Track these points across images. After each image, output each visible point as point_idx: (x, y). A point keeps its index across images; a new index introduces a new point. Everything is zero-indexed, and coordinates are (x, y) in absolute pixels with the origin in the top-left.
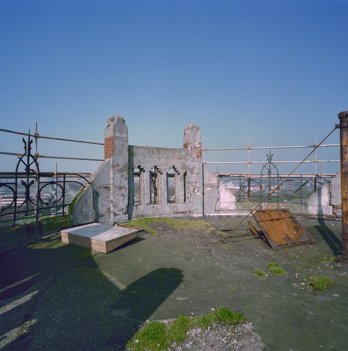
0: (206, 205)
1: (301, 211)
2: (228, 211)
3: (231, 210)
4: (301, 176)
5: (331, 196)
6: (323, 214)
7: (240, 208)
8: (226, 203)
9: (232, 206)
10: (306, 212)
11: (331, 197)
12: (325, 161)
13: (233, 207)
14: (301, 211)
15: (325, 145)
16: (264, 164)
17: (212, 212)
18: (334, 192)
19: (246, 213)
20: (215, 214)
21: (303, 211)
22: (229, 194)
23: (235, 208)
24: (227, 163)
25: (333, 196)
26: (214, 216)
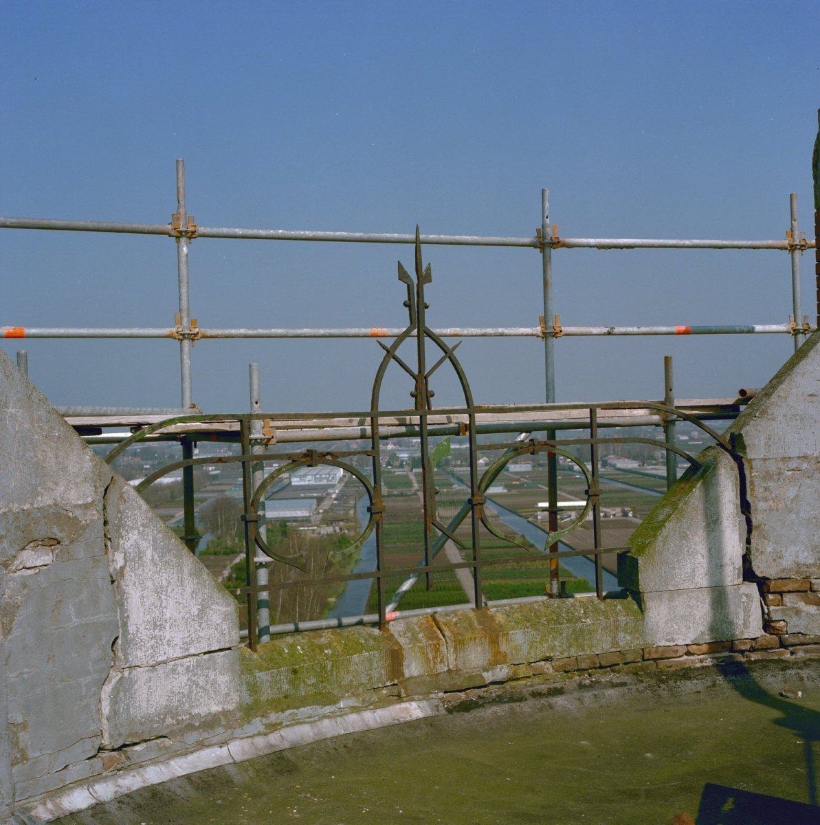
0: (24, 726)
1: (615, 642)
2: (192, 737)
3: (210, 723)
4: (592, 413)
5: (749, 521)
6: (707, 638)
7: (267, 694)
8: (174, 671)
9: (215, 682)
10: (639, 643)
11: (750, 531)
12: (595, 330)
13: (219, 692)
14: (615, 642)
15: (592, 241)
16: (389, 343)
17: (75, 772)
18: (766, 500)
19: (310, 720)
20: (105, 791)
21: (625, 640)
22: (190, 585)
23: (235, 697)
24: (28, 331)
25: (758, 527)
26: (98, 809)
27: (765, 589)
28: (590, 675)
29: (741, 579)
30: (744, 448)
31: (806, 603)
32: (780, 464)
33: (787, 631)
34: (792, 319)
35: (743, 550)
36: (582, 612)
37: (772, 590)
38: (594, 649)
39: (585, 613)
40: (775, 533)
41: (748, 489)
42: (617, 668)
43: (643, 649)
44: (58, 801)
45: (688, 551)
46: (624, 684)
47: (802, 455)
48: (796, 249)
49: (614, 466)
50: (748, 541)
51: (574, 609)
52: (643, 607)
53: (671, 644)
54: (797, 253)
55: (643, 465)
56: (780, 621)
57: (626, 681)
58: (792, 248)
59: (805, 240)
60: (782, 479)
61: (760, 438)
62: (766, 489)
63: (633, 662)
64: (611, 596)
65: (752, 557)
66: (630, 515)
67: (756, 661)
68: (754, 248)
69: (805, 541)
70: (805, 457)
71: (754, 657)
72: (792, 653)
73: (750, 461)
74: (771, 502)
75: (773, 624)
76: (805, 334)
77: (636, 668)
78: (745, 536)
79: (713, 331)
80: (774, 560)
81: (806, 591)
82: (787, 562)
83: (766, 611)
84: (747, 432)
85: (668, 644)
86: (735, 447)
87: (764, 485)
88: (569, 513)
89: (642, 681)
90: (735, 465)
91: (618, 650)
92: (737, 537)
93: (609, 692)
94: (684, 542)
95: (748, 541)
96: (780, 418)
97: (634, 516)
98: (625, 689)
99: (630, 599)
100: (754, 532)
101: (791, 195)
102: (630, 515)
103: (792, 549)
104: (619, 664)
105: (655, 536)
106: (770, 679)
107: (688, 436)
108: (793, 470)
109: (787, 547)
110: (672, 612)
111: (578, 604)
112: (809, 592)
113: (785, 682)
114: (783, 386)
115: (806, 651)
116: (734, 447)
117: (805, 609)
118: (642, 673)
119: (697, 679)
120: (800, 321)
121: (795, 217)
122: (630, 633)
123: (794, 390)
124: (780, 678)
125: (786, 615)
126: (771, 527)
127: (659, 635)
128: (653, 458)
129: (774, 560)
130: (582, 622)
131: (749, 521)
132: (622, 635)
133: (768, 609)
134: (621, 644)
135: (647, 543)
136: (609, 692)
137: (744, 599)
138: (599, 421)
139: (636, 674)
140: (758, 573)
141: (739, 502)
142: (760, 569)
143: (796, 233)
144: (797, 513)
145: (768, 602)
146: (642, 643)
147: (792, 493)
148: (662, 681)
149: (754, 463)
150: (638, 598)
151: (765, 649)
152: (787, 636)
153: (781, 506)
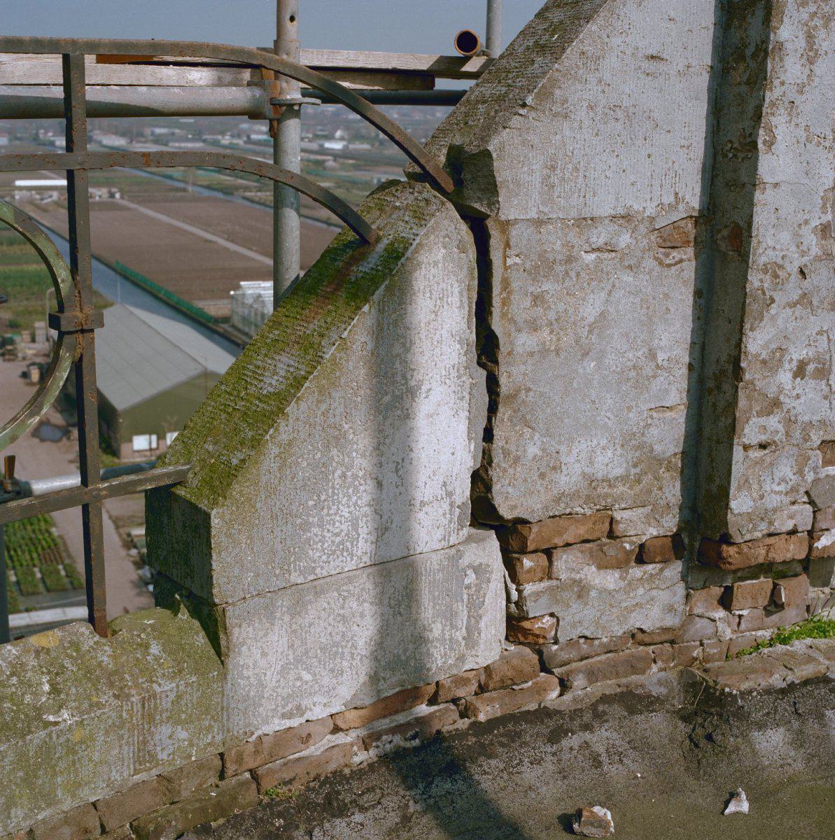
1: (144, 756)
5: (492, 384)
11: (493, 409)
14: (144, 756)
18: (534, 327)
21: (175, 743)
25: (512, 397)
27: (514, 544)
30: (491, 189)
31: (600, 567)
35: (474, 457)
36: (47, 688)
37: (531, 548)
39: (55, 690)
40: (549, 411)
41: (496, 301)
45: (344, 476)
47: (621, 211)
49: (100, 143)
50: (488, 435)
51: (21, 682)
52: (223, 643)
53: (295, 722)
55: (131, 142)
60: (573, 274)
62: (538, 299)
65: (494, 473)
66: (118, 196)
67: (493, 723)
69: (610, 423)
70: (626, 217)
73: (505, 226)
75: (526, 625)
78: (483, 423)
80: (542, 476)
82: (568, 479)
83: (515, 595)
84: (501, 149)
85: (288, 723)
86: (467, 182)
87: (531, 289)
88: (50, 193)
90: (464, 232)
92: (462, 427)
94: (334, 452)
95: (488, 435)
96: (582, 114)
97: (122, 197)
99: (184, 615)
100: (501, 409)
102: (118, 196)
103: (582, 446)
105: (257, 443)
106: (530, 774)
107: (320, 142)
108: (598, 250)
109: (572, 440)
110: (297, 643)
111: (32, 662)
112: (604, 540)
114: (593, 27)
116: (459, 183)
117: (597, 581)
119: (363, 809)
123: (616, 41)
126: (542, 395)
128: (142, 135)
130: (47, 724)
131: (492, 384)
133: (520, 592)
134: (163, 756)
135: (235, 461)
137: (471, 578)
138: (93, 95)
140: (506, 512)
142: (507, 504)
146: (219, 738)
147: (590, 311)
149: (514, 232)
150: (212, 622)
151: (507, 685)
152: (555, 647)
153: (567, 340)
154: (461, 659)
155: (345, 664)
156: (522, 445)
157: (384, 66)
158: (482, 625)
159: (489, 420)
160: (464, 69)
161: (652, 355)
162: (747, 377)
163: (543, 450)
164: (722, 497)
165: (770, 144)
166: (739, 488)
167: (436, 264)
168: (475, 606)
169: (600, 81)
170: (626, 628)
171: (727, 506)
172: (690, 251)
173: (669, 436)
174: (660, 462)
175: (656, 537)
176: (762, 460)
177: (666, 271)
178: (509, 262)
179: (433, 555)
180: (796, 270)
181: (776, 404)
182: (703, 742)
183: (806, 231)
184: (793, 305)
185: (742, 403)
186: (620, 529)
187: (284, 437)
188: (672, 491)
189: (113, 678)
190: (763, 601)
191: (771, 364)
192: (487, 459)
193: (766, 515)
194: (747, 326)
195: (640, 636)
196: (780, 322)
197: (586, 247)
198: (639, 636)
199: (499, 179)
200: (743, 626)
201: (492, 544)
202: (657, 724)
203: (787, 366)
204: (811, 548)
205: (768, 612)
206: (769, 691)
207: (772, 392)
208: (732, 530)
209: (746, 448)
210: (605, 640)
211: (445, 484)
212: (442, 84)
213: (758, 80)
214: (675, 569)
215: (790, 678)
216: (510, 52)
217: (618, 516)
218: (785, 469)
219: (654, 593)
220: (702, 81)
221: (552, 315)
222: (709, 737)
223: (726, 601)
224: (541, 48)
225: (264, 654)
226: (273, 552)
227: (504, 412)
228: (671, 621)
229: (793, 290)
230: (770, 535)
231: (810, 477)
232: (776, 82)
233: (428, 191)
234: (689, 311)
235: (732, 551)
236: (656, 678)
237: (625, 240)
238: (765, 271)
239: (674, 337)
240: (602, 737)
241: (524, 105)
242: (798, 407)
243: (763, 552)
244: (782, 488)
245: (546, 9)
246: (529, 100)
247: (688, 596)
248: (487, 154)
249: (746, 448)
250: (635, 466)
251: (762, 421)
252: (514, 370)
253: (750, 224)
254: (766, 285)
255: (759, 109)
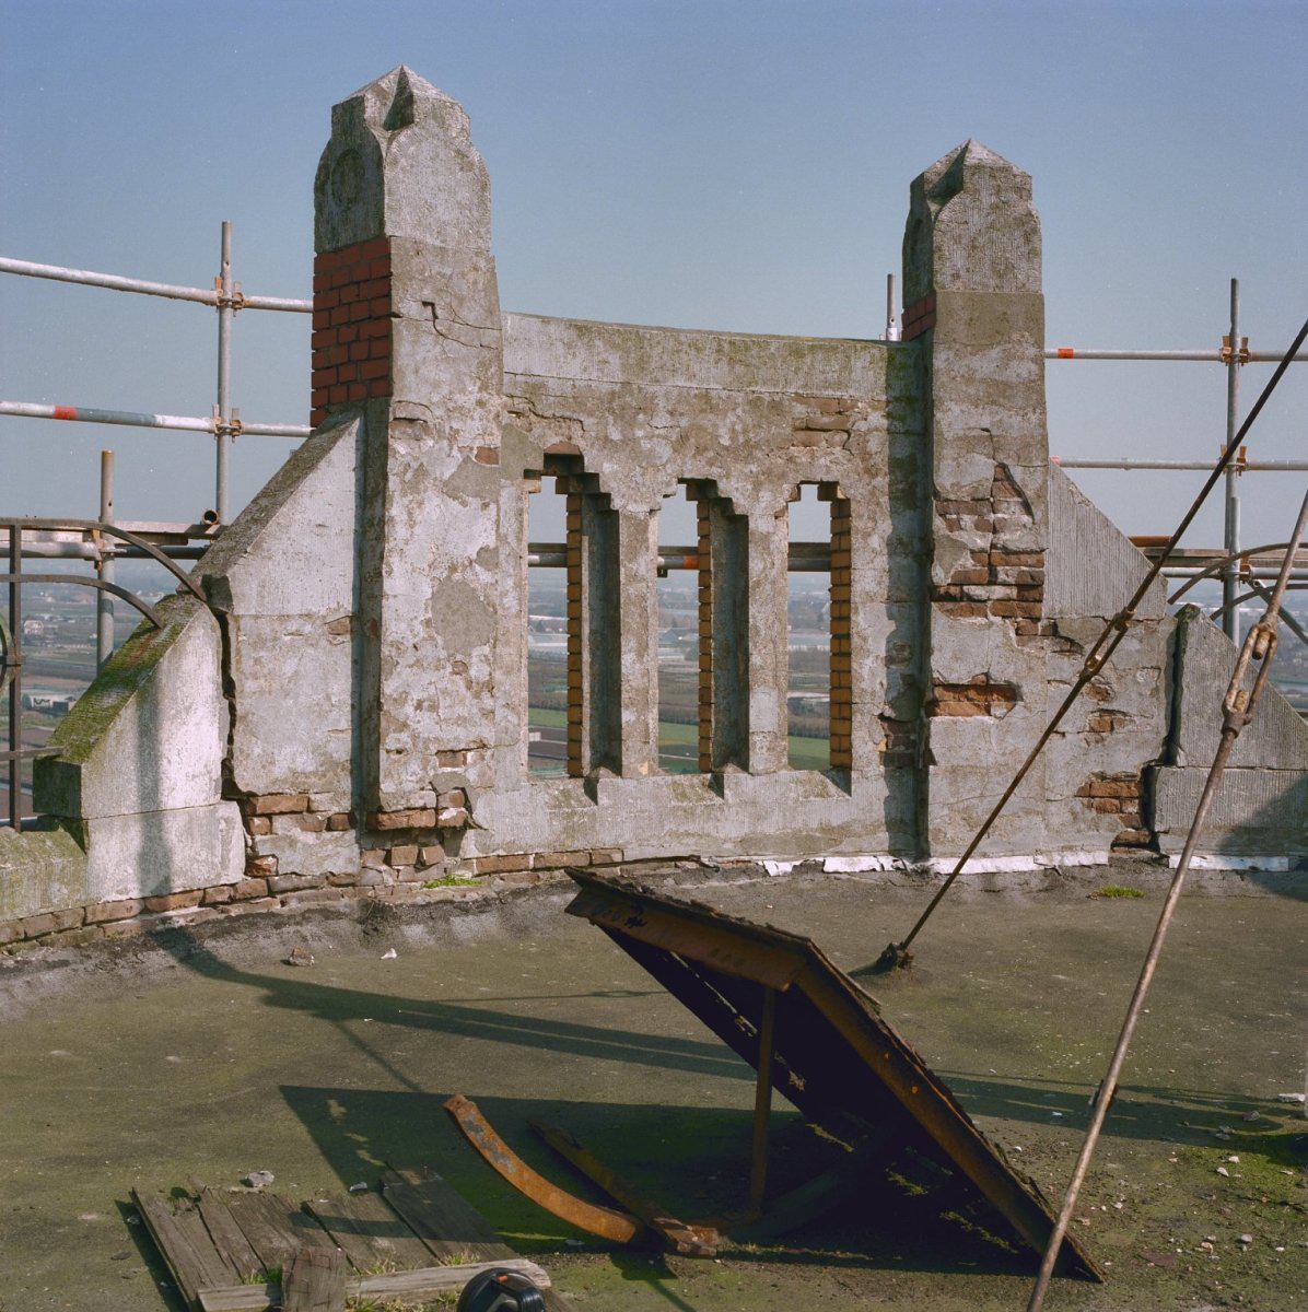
1: (46, 899)
5: (232, 709)
11: (233, 725)
14: (46, 899)
21: (61, 895)
28: (10, 952)
29: (219, 796)
30: (228, 598)
31: (303, 829)
32: (276, 625)
33: (277, 872)
34: (217, 411)
37: (259, 812)
38: (17, 911)
40: (266, 727)
41: (233, 661)
42: (48, 939)
43: (84, 908)
44: (1137, 801)
46: (65, 963)
48: (226, 306)
50: (231, 740)
52: (86, 842)
53: (124, 897)
54: (229, 312)
56: (268, 856)
57: (66, 958)
58: (222, 305)
59: (240, 294)
61: (256, 585)
63: (70, 929)
64: (27, 827)
67: (239, 917)
68: (171, 296)
70: (308, 616)
71: (235, 911)
72: (283, 903)
73: (237, 618)
74: (262, 681)
75: (258, 862)
76: (234, 436)
77: (75, 938)
79: (108, 419)
80: (264, 767)
81: (301, 812)
82: (279, 771)
85: (120, 897)
86: (215, 594)
89: (89, 957)
90: (217, 624)
91: (50, 910)
93: (47, 977)
95: (231, 740)
96: (279, 557)
98: (68, 969)
99: (61, 830)
101: (223, 223)
103: (288, 750)
104: (49, 933)
105: (104, 730)
108: (292, 634)
109: (281, 746)
110: (125, 849)
113: (284, 943)
114: (284, 510)
115: (301, 900)
118: (86, 944)
120: (227, 416)
121: (229, 256)
122: (67, 884)
124: (275, 939)
125: (276, 848)
127: (108, 885)
129: (264, 767)
131: (232, 709)
132: (56, 886)
133: (253, 839)
134: (55, 901)
136: (47, 977)
137: (223, 825)
139: (77, 946)
141: (220, 680)
142: (244, 781)
143: (229, 282)
144: (297, 696)
145: (254, 830)
147: (289, 667)
148: (116, 955)
149: (242, 622)
150: (78, 831)
151: (247, 899)
153: (276, 686)
154: (219, 876)
155: (151, 867)
156: (252, 750)
157: (159, 531)
158: (231, 855)
159: (231, 731)
160: (207, 532)
161: (328, 698)
162: (385, 708)
163: (264, 751)
164: (375, 784)
165: (390, 573)
166: (385, 776)
167: (199, 638)
168: (226, 843)
169: (289, 539)
170: (321, 871)
171: (379, 788)
172: (348, 636)
173: (342, 748)
174: (337, 764)
175: (339, 814)
176: (399, 760)
177: (334, 648)
178: (240, 639)
179: (201, 809)
180: (411, 645)
181: (405, 726)
182: (371, 932)
183: (416, 622)
184: (411, 666)
185: (383, 724)
186: (314, 806)
187: (119, 728)
188: (346, 784)
189: (30, 852)
190: (413, 861)
191: (401, 700)
192: (230, 753)
193: (405, 795)
194: (383, 677)
195: (331, 878)
196: (404, 676)
197: (285, 632)
198: (330, 878)
199: (233, 592)
200: (400, 877)
201: (234, 806)
202: (344, 926)
203: (410, 703)
204: (437, 820)
205: (418, 870)
206: (413, 905)
207: (402, 718)
208: (383, 803)
209: (388, 752)
210: (309, 877)
211: (206, 766)
212: (193, 544)
213: (381, 538)
214: (351, 835)
215: (428, 899)
216: (237, 523)
217: (312, 797)
218: (415, 766)
219: (339, 849)
220: (350, 539)
221: (266, 671)
222: (376, 929)
223: (387, 861)
224: (255, 521)
225: (107, 852)
226: (112, 792)
227: (239, 727)
228: (351, 869)
229: (410, 657)
230: (409, 809)
231: (432, 773)
232: (391, 539)
233: (192, 599)
234: (350, 672)
235: (385, 817)
236: (346, 902)
237: (308, 629)
238: (392, 646)
239: (341, 687)
240: (307, 929)
241: (246, 552)
242: (420, 728)
243: (405, 819)
244: (413, 778)
245: (258, 498)
246: (248, 550)
247: (361, 853)
248: (226, 579)
249: (388, 752)
250: (321, 765)
251: (396, 735)
252: (245, 702)
253: (381, 619)
254: (393, 654)
255: (382, 553)
